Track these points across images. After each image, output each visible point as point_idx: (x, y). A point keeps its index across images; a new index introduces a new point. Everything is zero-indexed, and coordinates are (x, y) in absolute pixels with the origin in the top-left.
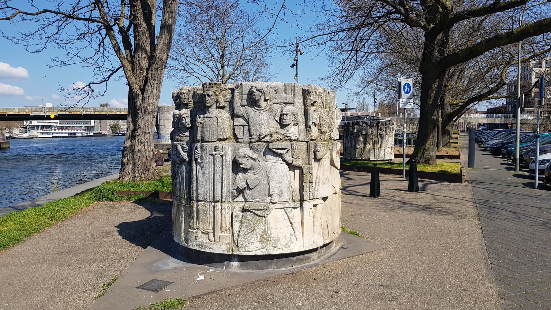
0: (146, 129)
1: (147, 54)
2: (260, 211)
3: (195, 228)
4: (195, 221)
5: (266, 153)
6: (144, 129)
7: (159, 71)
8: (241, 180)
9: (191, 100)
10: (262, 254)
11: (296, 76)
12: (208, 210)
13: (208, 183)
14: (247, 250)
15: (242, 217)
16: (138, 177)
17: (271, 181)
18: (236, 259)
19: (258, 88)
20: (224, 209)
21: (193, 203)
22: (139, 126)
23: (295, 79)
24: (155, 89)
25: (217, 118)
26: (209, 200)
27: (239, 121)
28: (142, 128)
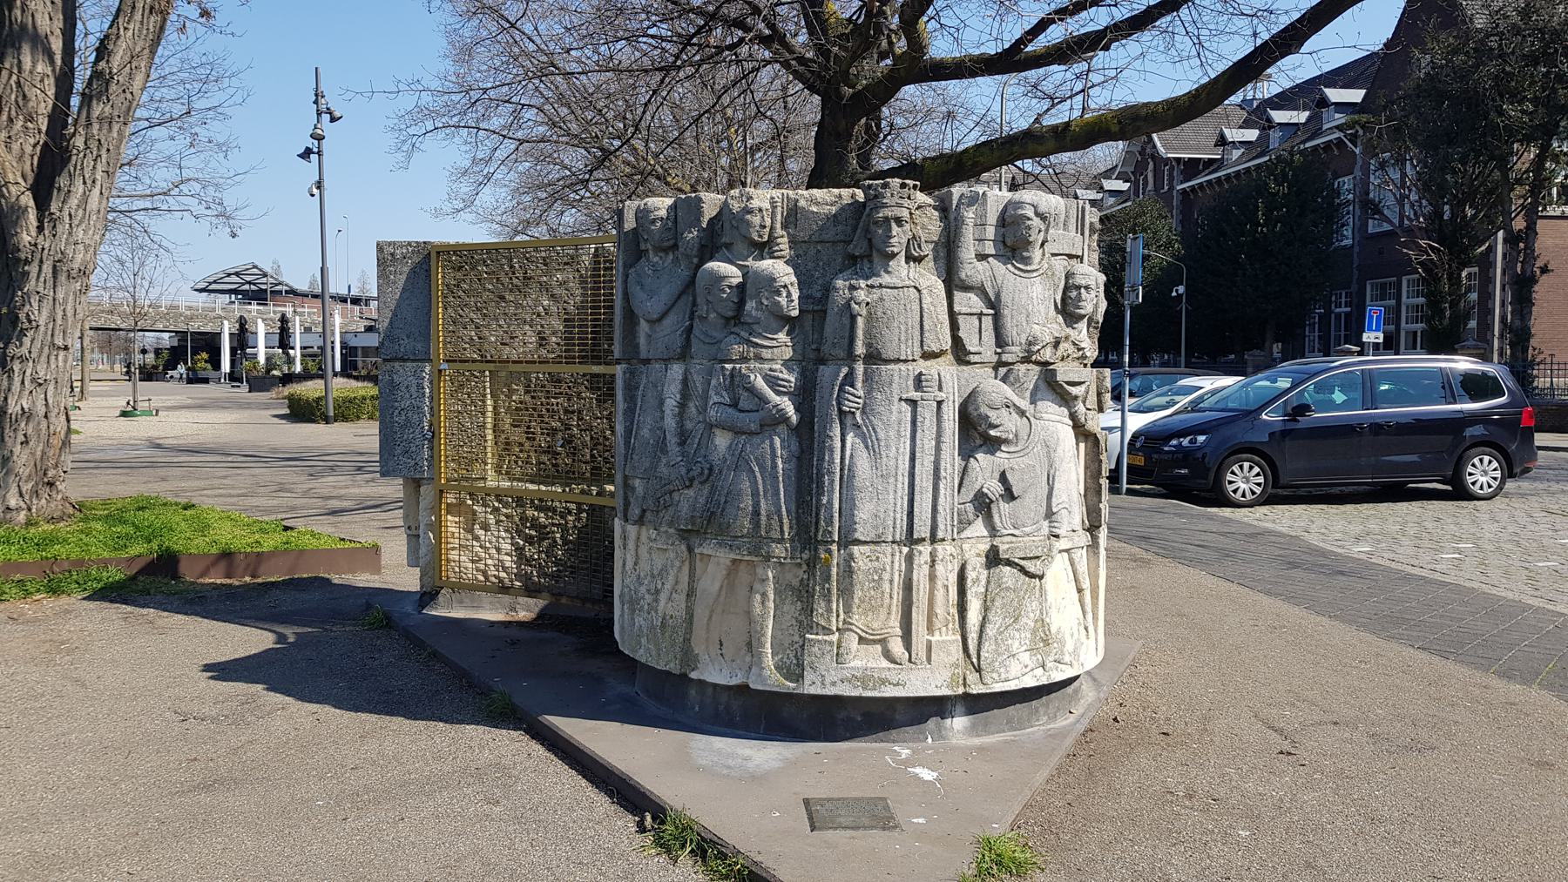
0: (57, 332)
1: (52, 62)
2: (1033, 561)
3: (835, 629)
4: (834, 606)
5: (1039, 396)
6: (50, 333)
7: (116, 127)
8: (985, 468)
9: (779, 231)
10: (1037, 684)
11: (319, 188)
12: (888, 568)
13: (891, 489)
14: (1003, 676)
15: (988, 582)
16: (18, 509)
17: (1057, 473)
18: (959, 708)
19: (1042, 209)
20: (942, 560)
21: (829, 552)
22: (30, 321)
23: (313, 195)
24: (96, 191)
25: (919, 291)
26: (890, 539)
27: (968, 302)
28: (42, 329)
